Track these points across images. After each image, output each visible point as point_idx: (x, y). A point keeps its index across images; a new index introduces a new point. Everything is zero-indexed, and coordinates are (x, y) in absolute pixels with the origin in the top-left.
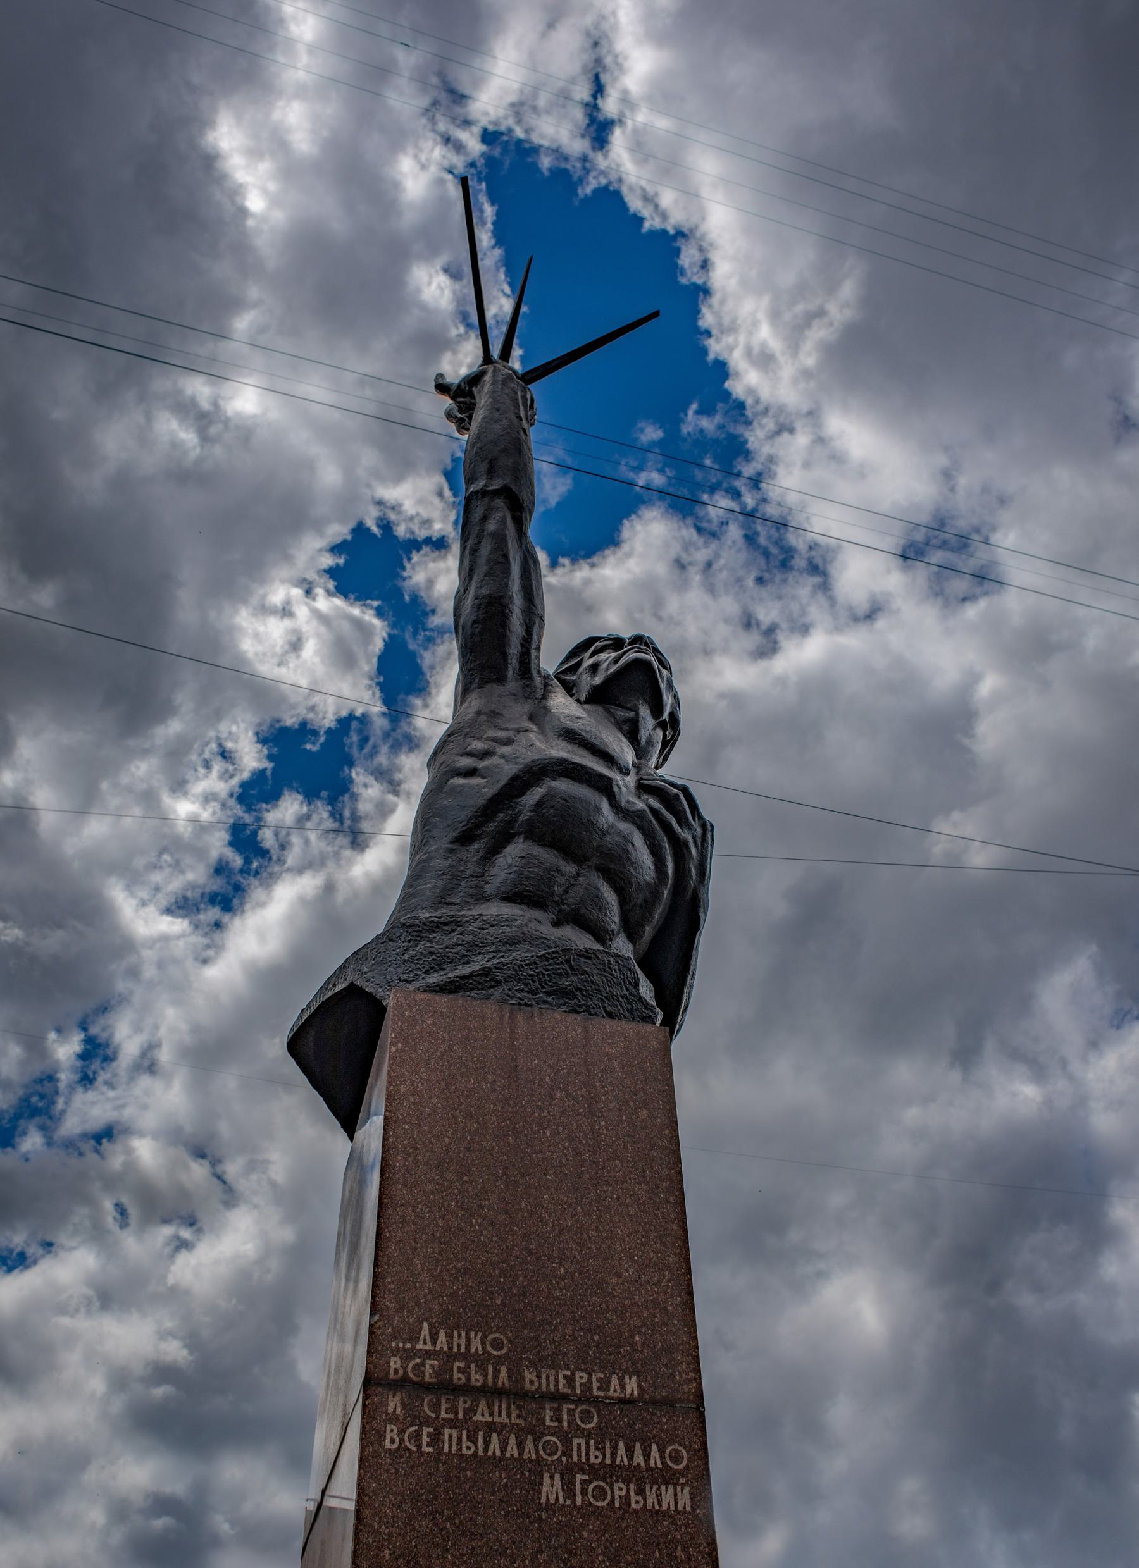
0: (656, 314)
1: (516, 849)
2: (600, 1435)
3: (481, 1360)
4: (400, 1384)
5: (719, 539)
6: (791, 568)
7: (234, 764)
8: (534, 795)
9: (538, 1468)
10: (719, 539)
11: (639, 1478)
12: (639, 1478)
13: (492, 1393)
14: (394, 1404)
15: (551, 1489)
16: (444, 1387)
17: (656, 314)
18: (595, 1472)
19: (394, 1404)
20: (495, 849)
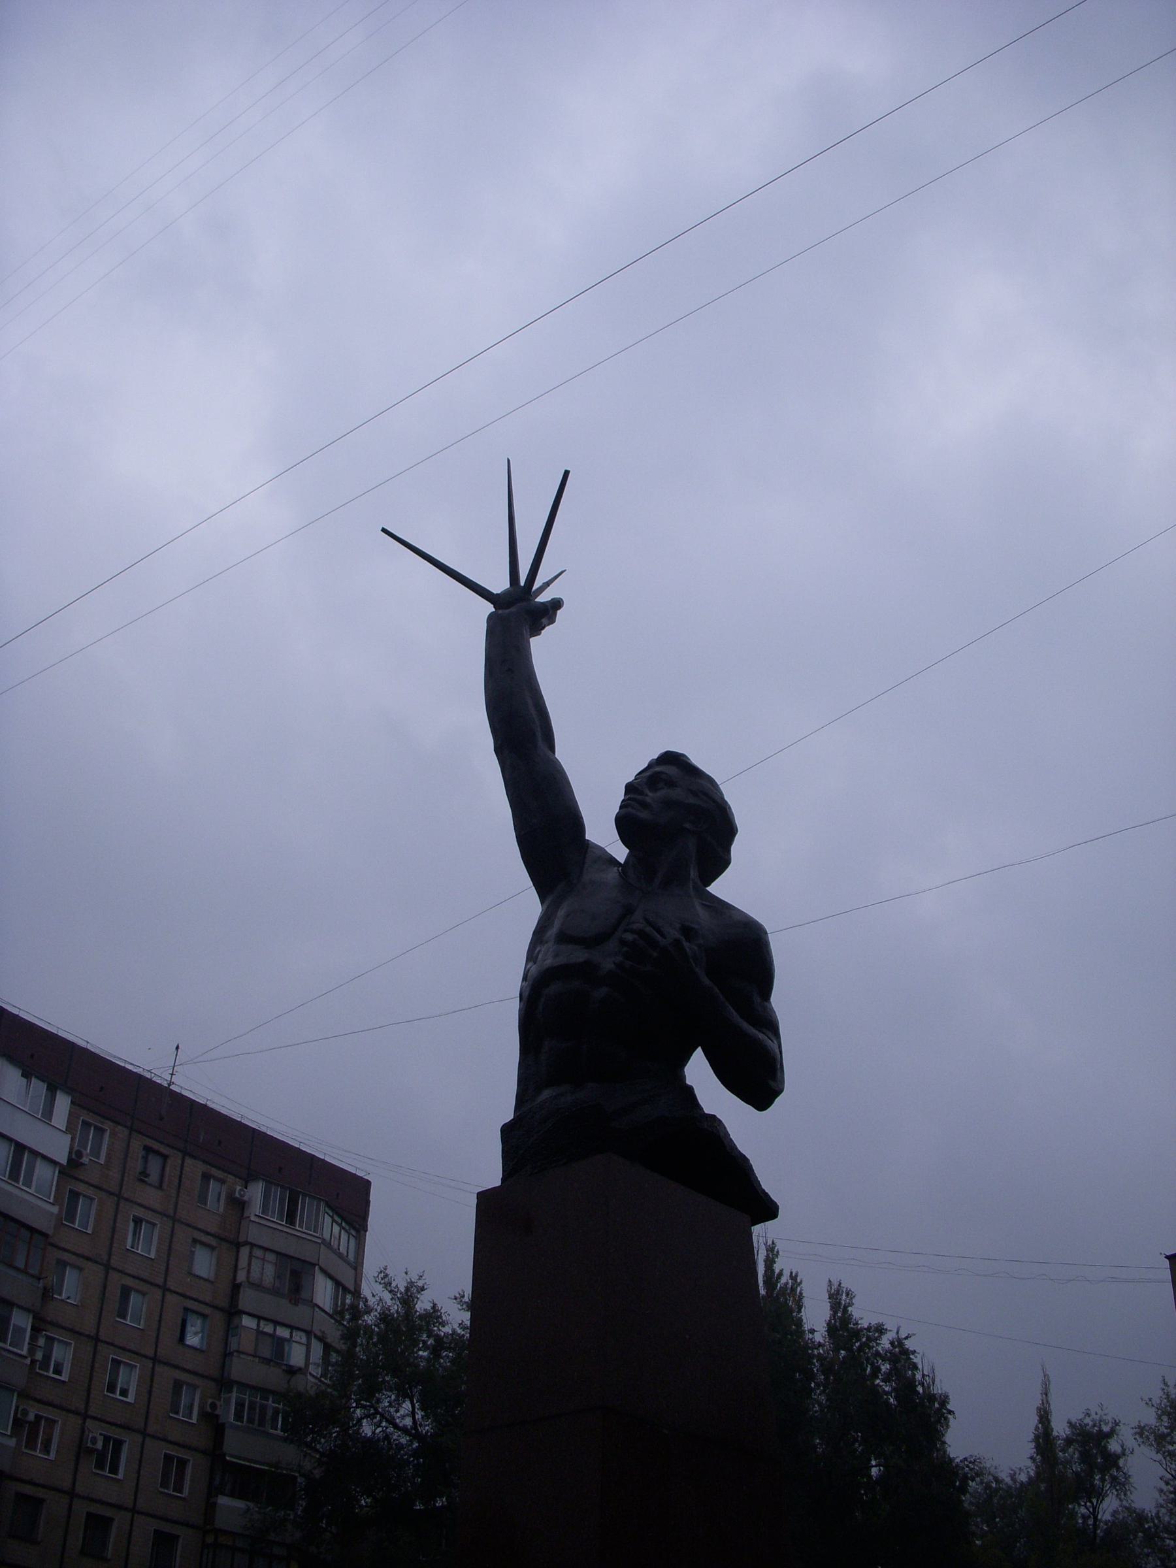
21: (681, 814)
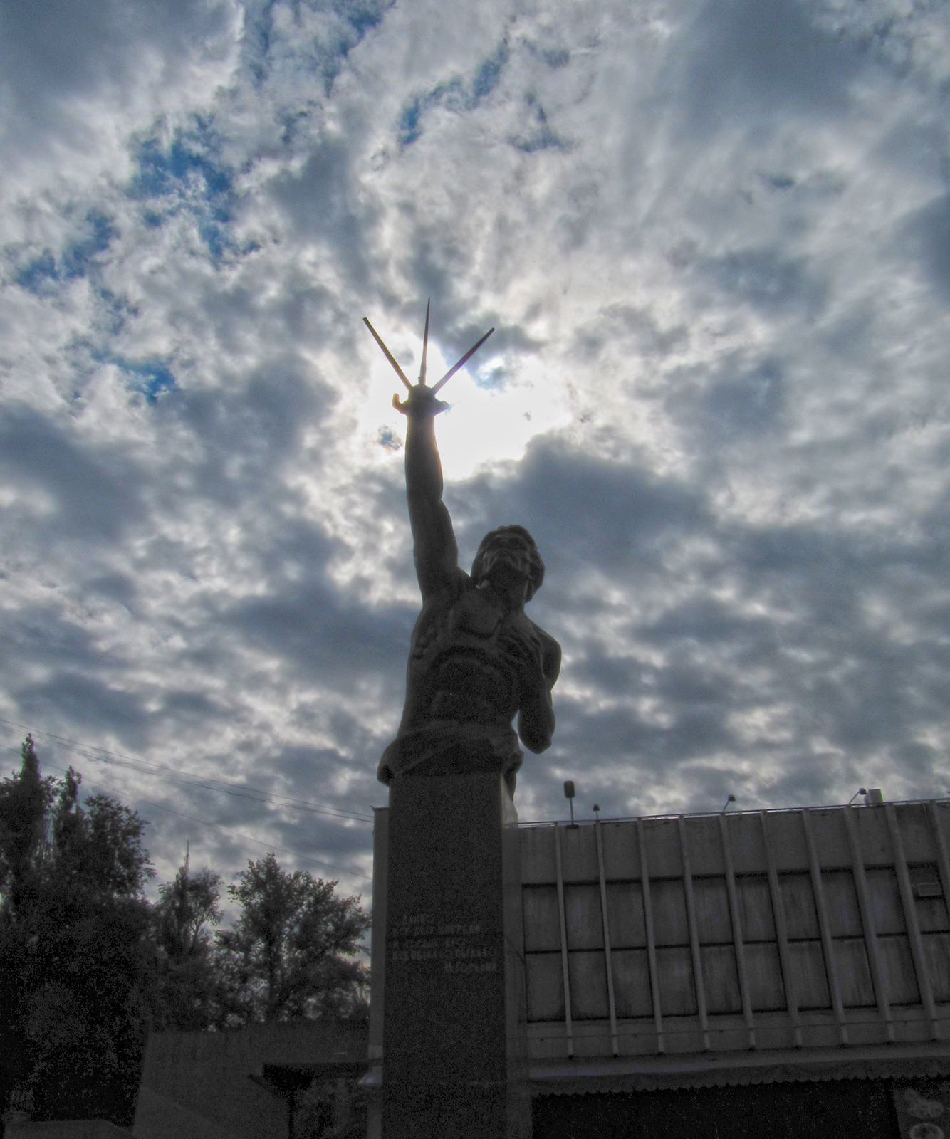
15: (448, 968)
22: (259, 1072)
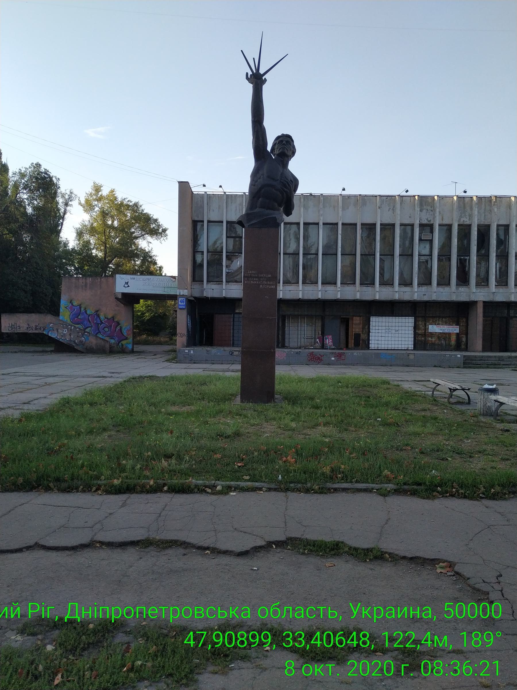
0: (254, 59)
1: (260, 199)
2: (266, 281)
3: (254, 274)
4: (247, 277)
5: (101, 186)
6: (165, 315)
7: (137, 256)
8: (263, 190)
9: (260, 284)
10: (101, 186)
11: (270, 285)
12: (270, 285)
13: (256, 277)
14: (246, 279)
15: (261, 286)
16: (251, 277)
17: (254, 59)
18: (265, 284)
19: (246, 279)
20: (258, 199)
21: (286, 145)
22: (120, 296)
